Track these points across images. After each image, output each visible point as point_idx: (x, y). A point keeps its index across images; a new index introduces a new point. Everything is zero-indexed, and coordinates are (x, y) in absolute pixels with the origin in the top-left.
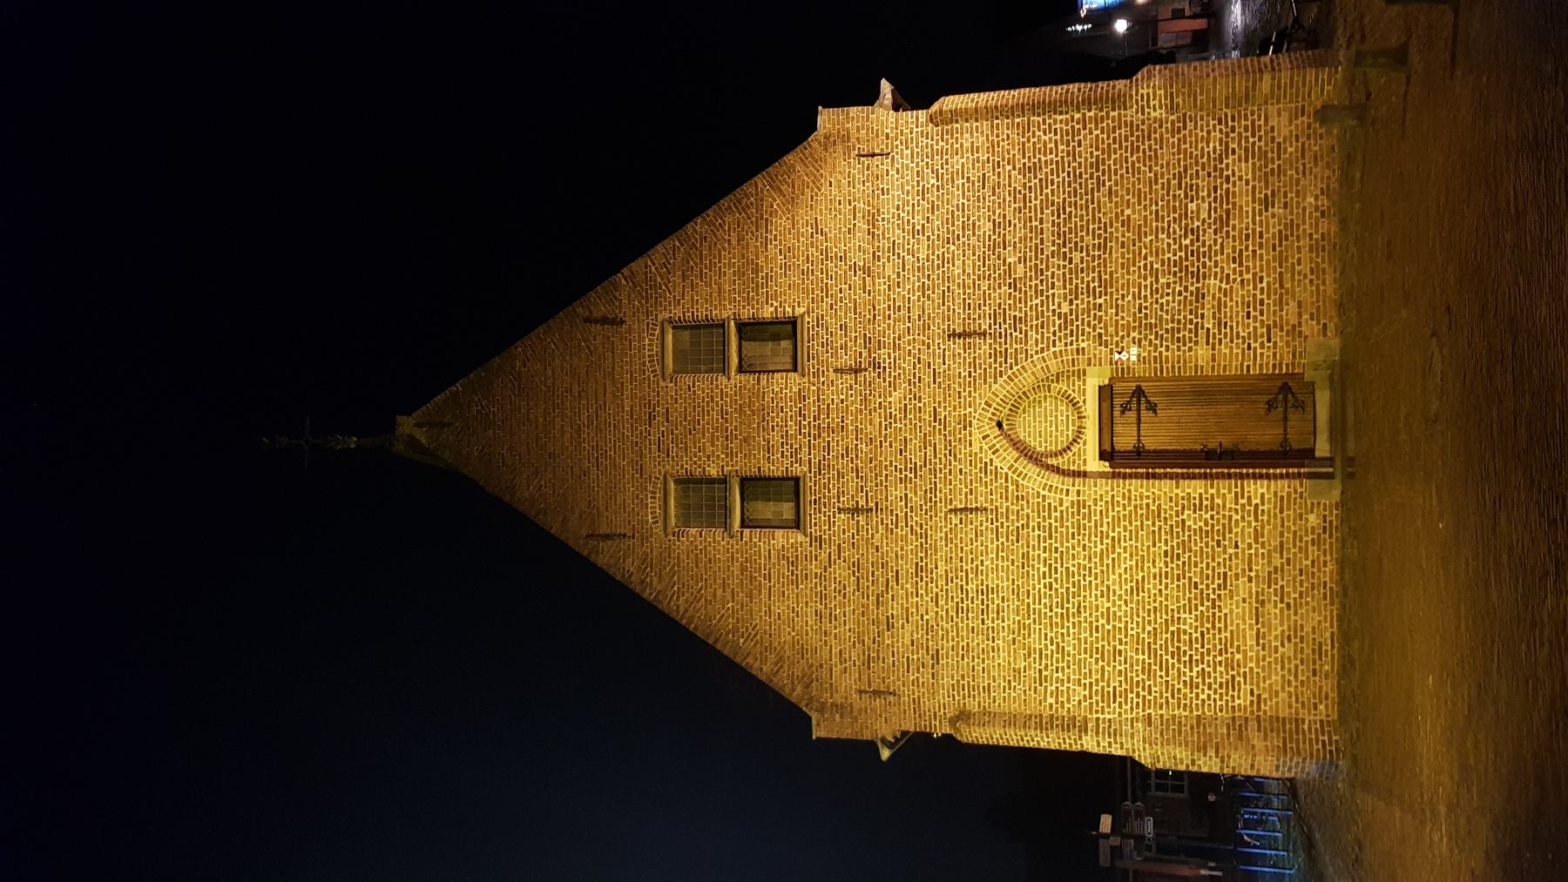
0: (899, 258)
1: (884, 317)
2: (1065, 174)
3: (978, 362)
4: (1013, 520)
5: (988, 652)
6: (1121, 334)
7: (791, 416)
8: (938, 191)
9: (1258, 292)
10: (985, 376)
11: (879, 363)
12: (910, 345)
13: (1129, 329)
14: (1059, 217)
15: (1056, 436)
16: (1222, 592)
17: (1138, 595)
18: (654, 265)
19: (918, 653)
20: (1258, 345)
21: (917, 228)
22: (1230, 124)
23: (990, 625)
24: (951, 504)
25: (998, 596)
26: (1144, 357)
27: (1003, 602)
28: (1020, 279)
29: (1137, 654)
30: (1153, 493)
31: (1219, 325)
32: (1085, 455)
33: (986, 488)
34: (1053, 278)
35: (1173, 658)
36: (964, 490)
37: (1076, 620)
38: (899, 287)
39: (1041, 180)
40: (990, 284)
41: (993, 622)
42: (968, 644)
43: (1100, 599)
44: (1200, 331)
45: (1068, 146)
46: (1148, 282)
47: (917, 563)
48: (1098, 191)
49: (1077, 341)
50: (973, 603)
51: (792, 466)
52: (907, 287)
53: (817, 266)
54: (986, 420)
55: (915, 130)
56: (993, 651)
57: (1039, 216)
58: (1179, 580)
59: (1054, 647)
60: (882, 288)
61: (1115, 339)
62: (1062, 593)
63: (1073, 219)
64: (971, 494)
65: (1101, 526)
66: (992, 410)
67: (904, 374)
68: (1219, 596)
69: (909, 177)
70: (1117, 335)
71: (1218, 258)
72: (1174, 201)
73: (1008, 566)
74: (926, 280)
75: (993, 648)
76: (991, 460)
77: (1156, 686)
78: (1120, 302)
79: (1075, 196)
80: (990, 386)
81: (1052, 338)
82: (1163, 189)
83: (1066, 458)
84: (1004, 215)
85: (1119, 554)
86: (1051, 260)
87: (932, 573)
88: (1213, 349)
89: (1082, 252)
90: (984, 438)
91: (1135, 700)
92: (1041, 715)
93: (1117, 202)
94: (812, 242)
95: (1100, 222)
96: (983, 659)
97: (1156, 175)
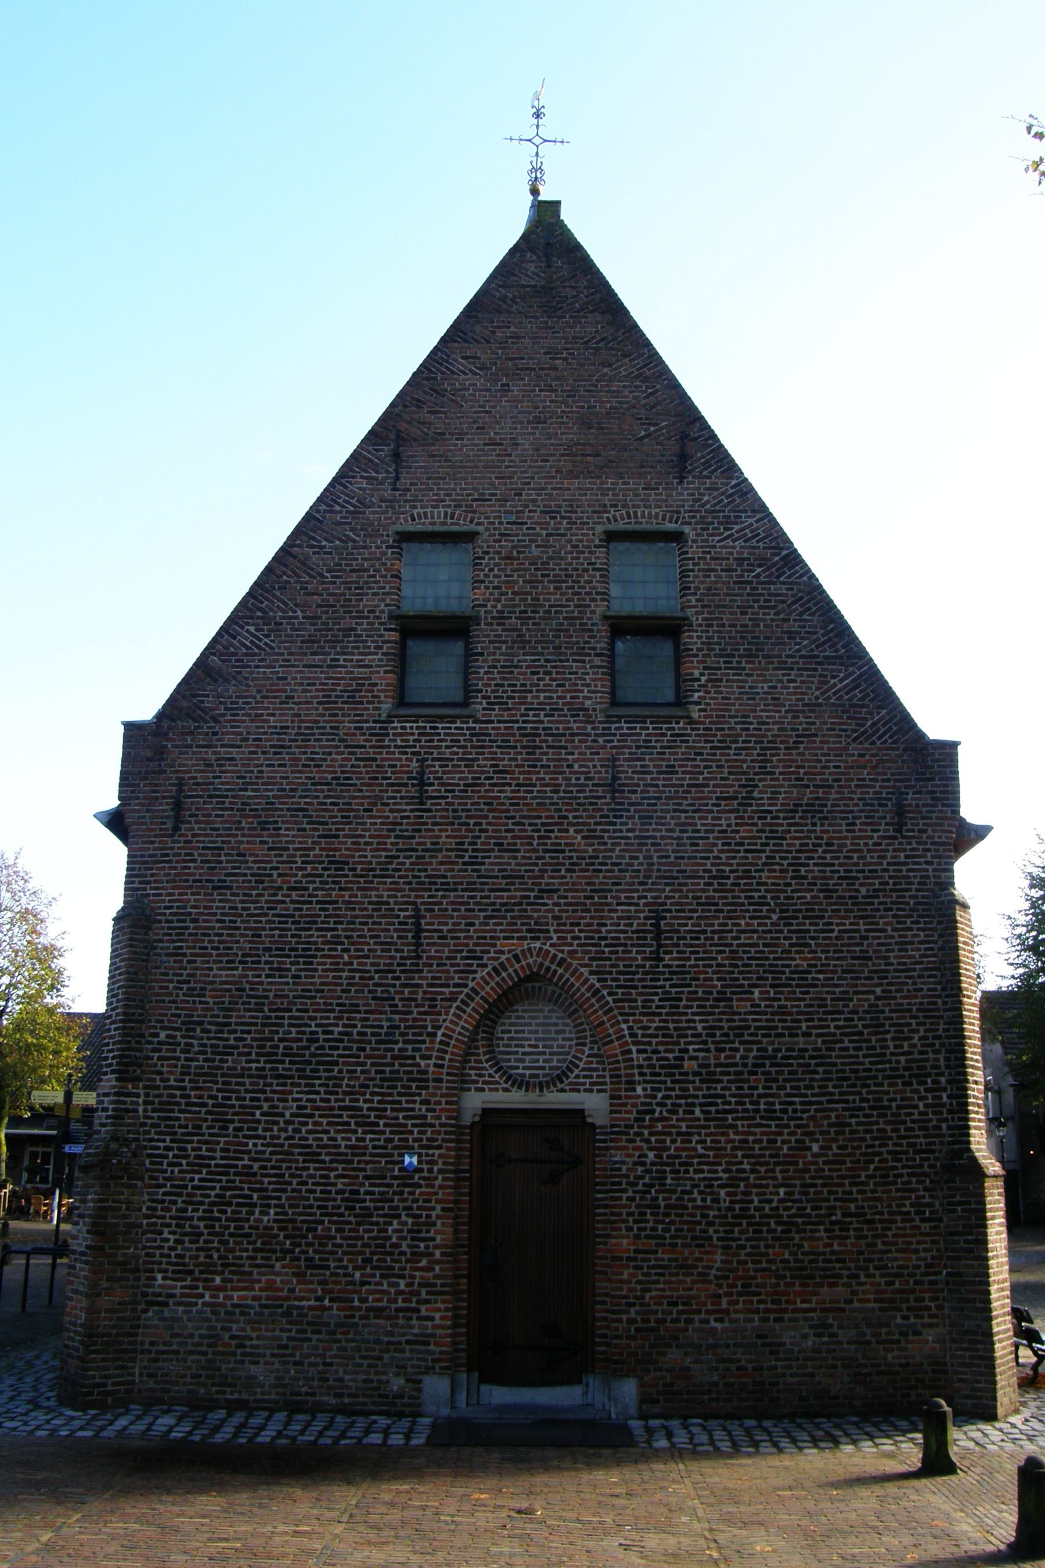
0: (762, 845)
1: (683, 824)
2: (868, 1066)
3: (620, 949)
4: (402, 993)
5: (227, 955)
6: (653, 1139)
7: (551, 698)
8: (851, 898)
9: (703, 1316)
10: (600, 959)
11: (621, 817)
12: (645, 858)
13: (660, 1149)
14: (811, 1057)
15: (516, 1053)
16: (303, 1264)
17: (300, 1154)
18: (757, 521)
19: (228, 861)
20: (633, 1315)
21: (803, 869)
22: (926, 1279)
23: (263, 959)
24: (426, 910)
25: (301, 970)
26: (620, 1169)
27: (294, 977)
28: (731, 1007)
29: (222, 1150)
30: (436, 1178)
31: (661, 1267)
32: (490, 1090)
33: (448, 958)
34: (731, 1049)
35: (216, 1196)
36: (445, 928)
37: (267, 1072)
38: (723, 844)
39: (861, 1033)
40: (724, 965)
41: (266, 962)
42: (239, 928)
43: (295, 1104)
44: (653, 1242)
45: (905, 1069)
46: (721, 1175)
47: (347, 863)
48: (844, 1109)
49: (645, 1082)
50: (293, 936)
51: (483, 697)
52: (723, 856)
53: (754, 735)
54: (540, 960)
55: (930, 868)
56: (228, 962)
57: (814, 1031)
58: (319, 1207)
59: (232, 1042)
60: (723, 822)
61: (646, 1132)
62: (304, 1055)
63: (808, 1076)
64: (439, 938)
65: (392, 1110)
66: (553, 967)
67: (605, 851)
68: (298, 1259)
69: (869, 860)
70: (651, 1134)
71: (750, 1265)
72: (828, 1208)
73: (341, 984)
74: (732, 881)
75: (233, 962)
76: (486, 965)
77: (180, 1172)
78: (696, 1138)
79: (838, 1079)
80: (586, 965)
81: (649, 1048)
82: (844, 1193)
83: (487, 1065)
84: (816, 986)
85: (355, 1132)
86: (755, 1047)
87: (333, 882)
88: (629, 1259)
89: (764, 1088)
90: (516, 957)
91: (161, 1144)
92: (142, 1022)
93: (829, 1133)
94: (785, 729)
95: (803, 1111)
96: (218, 948)
97: (863, 1184)
